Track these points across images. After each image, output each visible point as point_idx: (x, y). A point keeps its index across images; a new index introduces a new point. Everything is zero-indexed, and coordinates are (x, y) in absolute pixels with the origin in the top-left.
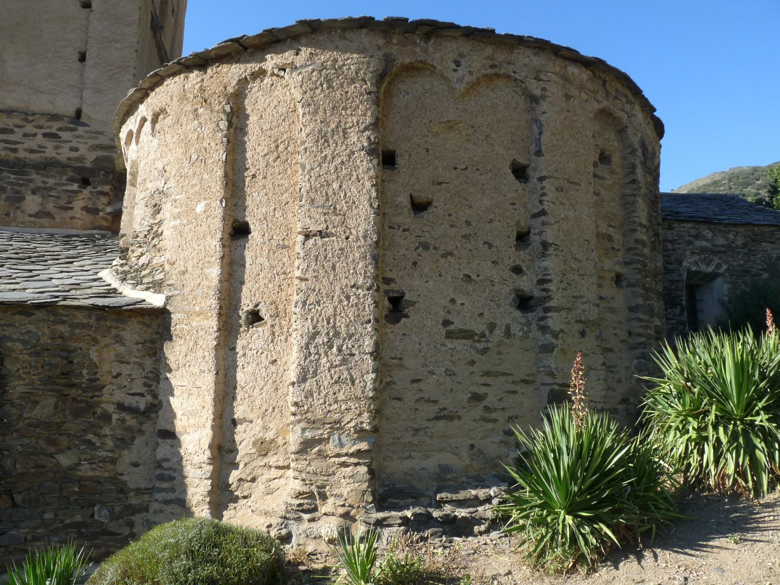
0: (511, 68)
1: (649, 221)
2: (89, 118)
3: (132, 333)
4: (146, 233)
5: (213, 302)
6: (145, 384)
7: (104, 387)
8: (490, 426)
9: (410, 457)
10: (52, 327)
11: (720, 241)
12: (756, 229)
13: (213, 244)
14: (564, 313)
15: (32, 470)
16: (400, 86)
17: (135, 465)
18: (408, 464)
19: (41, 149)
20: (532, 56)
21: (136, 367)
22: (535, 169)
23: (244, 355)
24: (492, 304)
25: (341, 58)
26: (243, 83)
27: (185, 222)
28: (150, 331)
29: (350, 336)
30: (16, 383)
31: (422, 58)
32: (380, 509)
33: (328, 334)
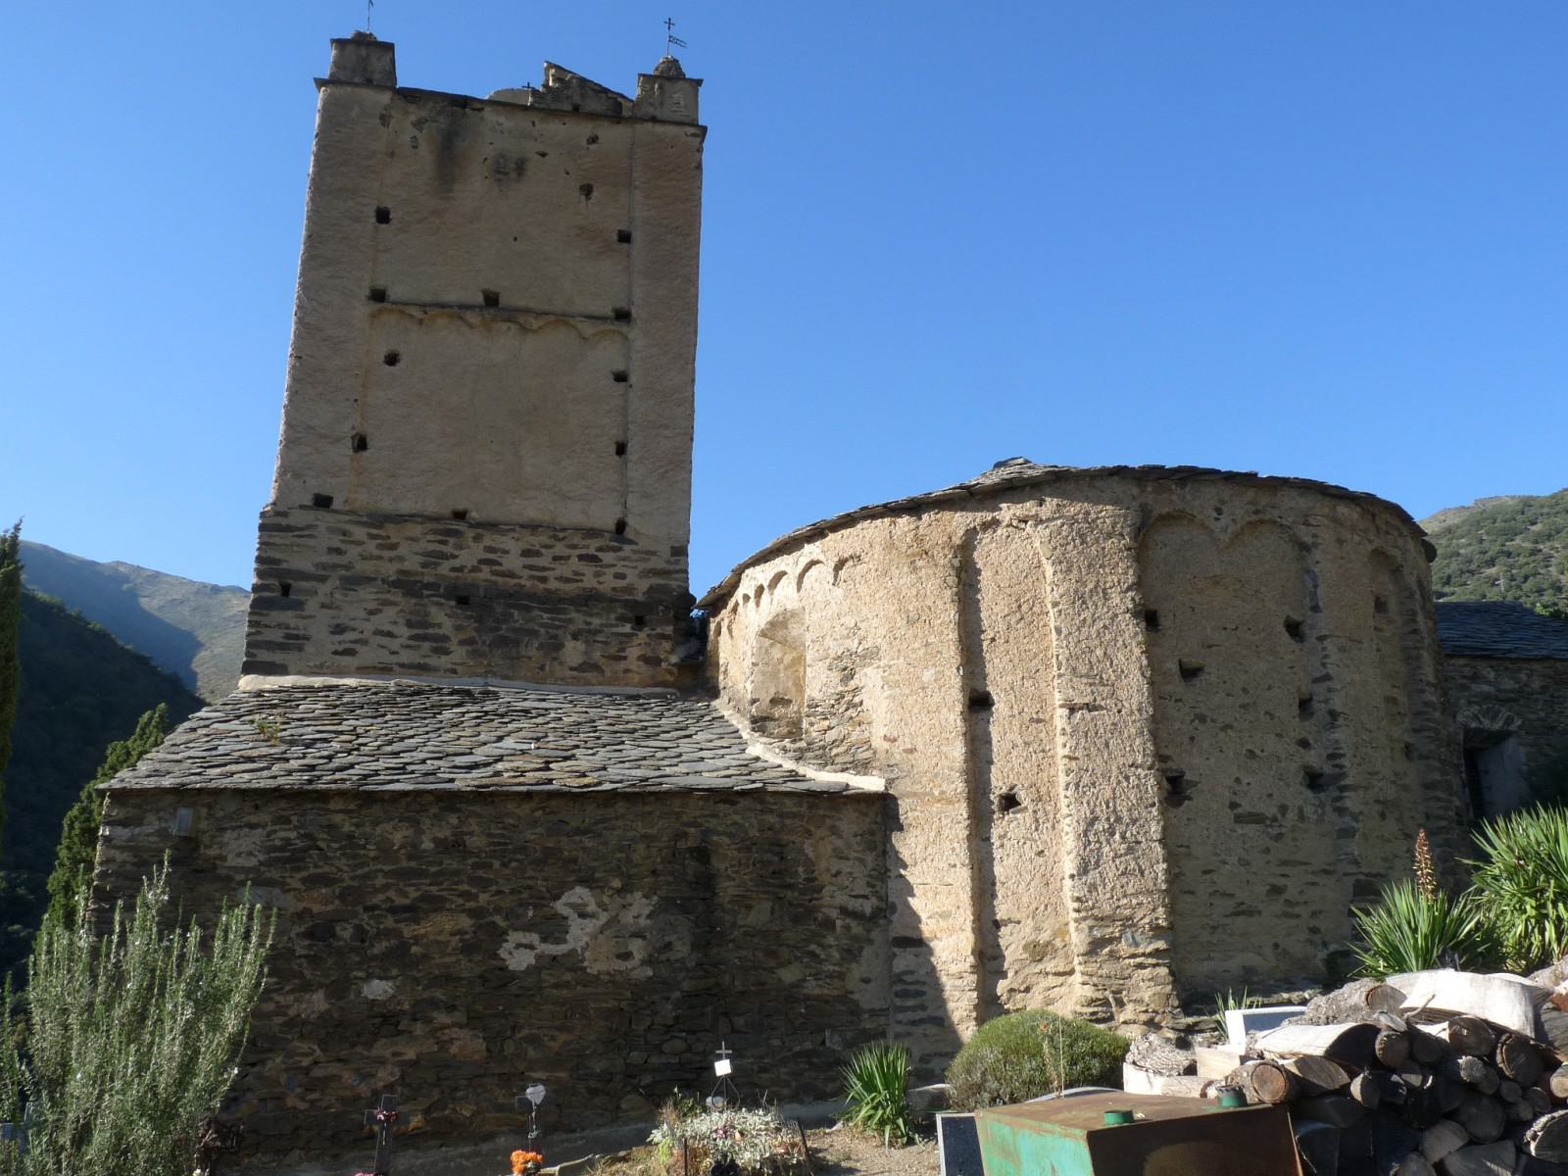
0: (1276, 513)
1: (1436, 677)
2: (637, 533)
3: (849, 823)
4: (833, 702)
5: (959, 786)
6: (869, 885)
7: (823, 887)
8: (1293, 922)
9: (1210, 958)
10: (760, 817)
11: (1508, 684)
12: (1559, 665)
13: (952, 717)
14: (1361, 792)
15: (753, 988)
16: (1155, 537)
17: (866, 981)
18: (1206, 967)
20: (1298, 498)
21: (857, 863)
22: (1312, 627)
23: (1002, 846)
24: (1281, 783)
25: (1093, 510)
26: (971, 534)
27: (907, 691)
28: (868, 820)
29: (1134, 821)
30: (726, 884)
31: (1180, 507)
32: (1188, 1014)
33: (1108, 819)
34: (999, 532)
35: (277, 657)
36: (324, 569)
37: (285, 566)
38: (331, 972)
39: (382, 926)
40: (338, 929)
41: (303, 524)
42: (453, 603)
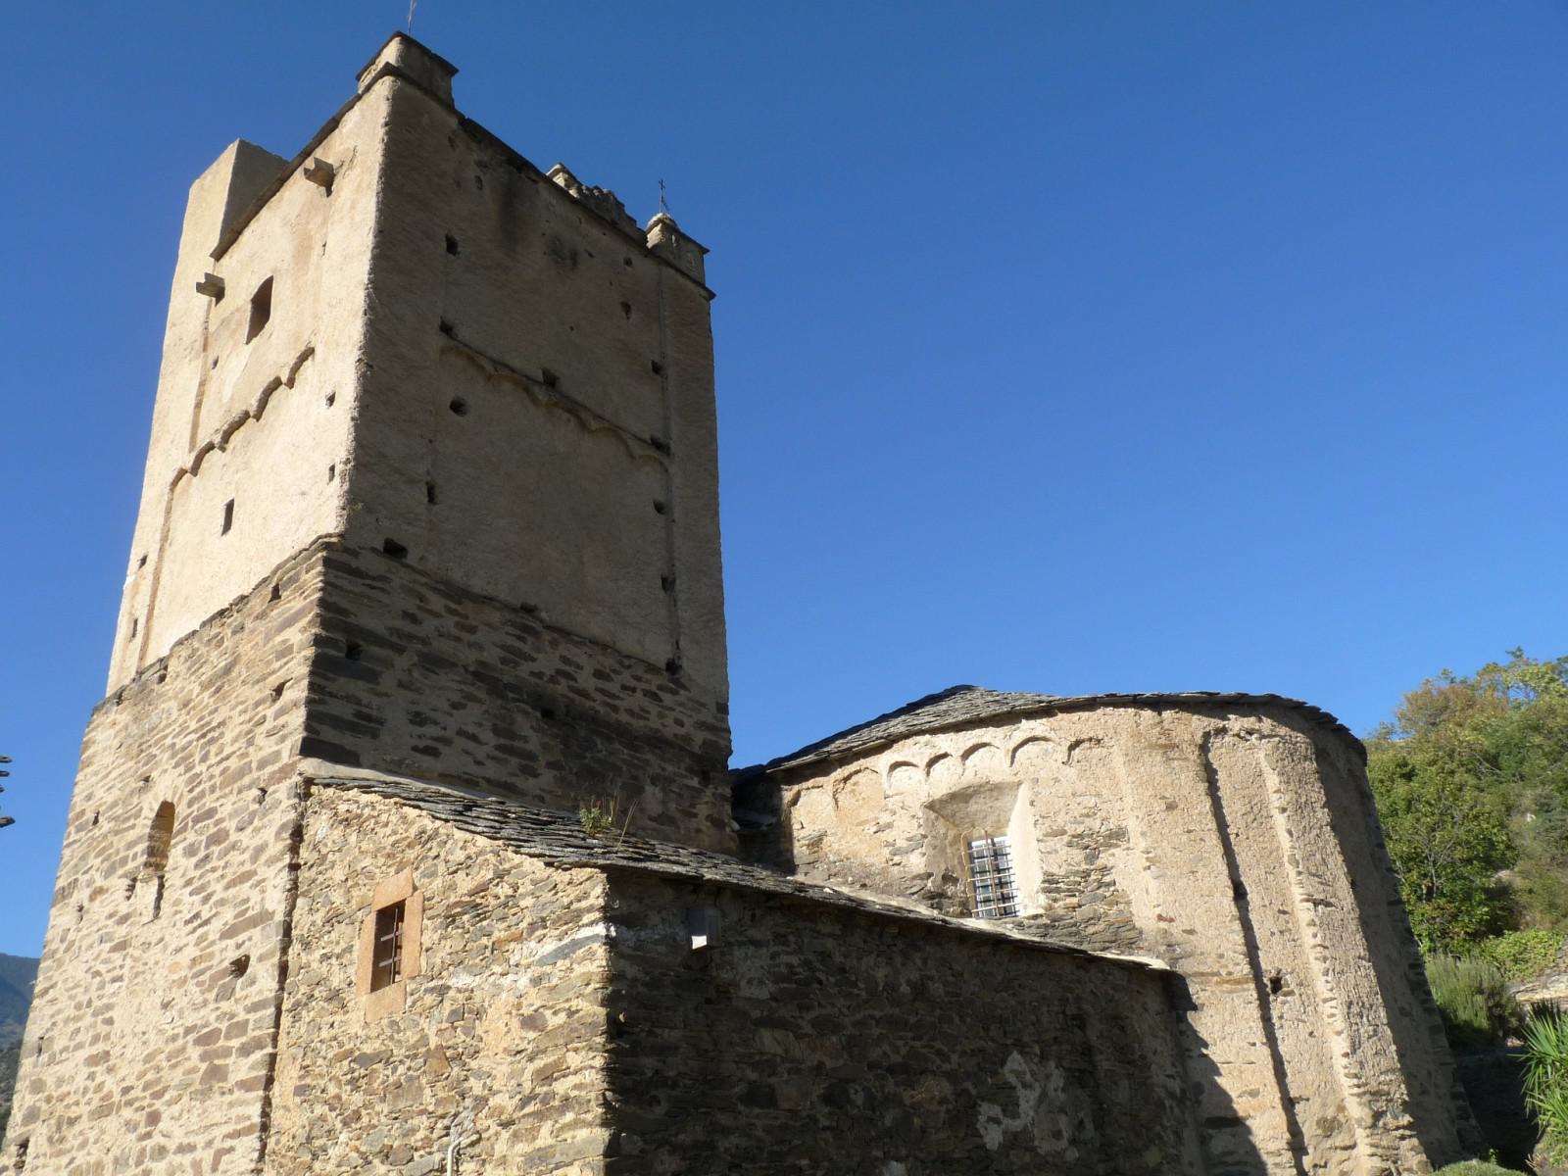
5: (1246, 969)
19: (641, 714)
23: (1282, 1027)
34: (1227, 739)
35: (347, 740)
36: (399, 637)
37: (352, 620)
42: (538, 714)
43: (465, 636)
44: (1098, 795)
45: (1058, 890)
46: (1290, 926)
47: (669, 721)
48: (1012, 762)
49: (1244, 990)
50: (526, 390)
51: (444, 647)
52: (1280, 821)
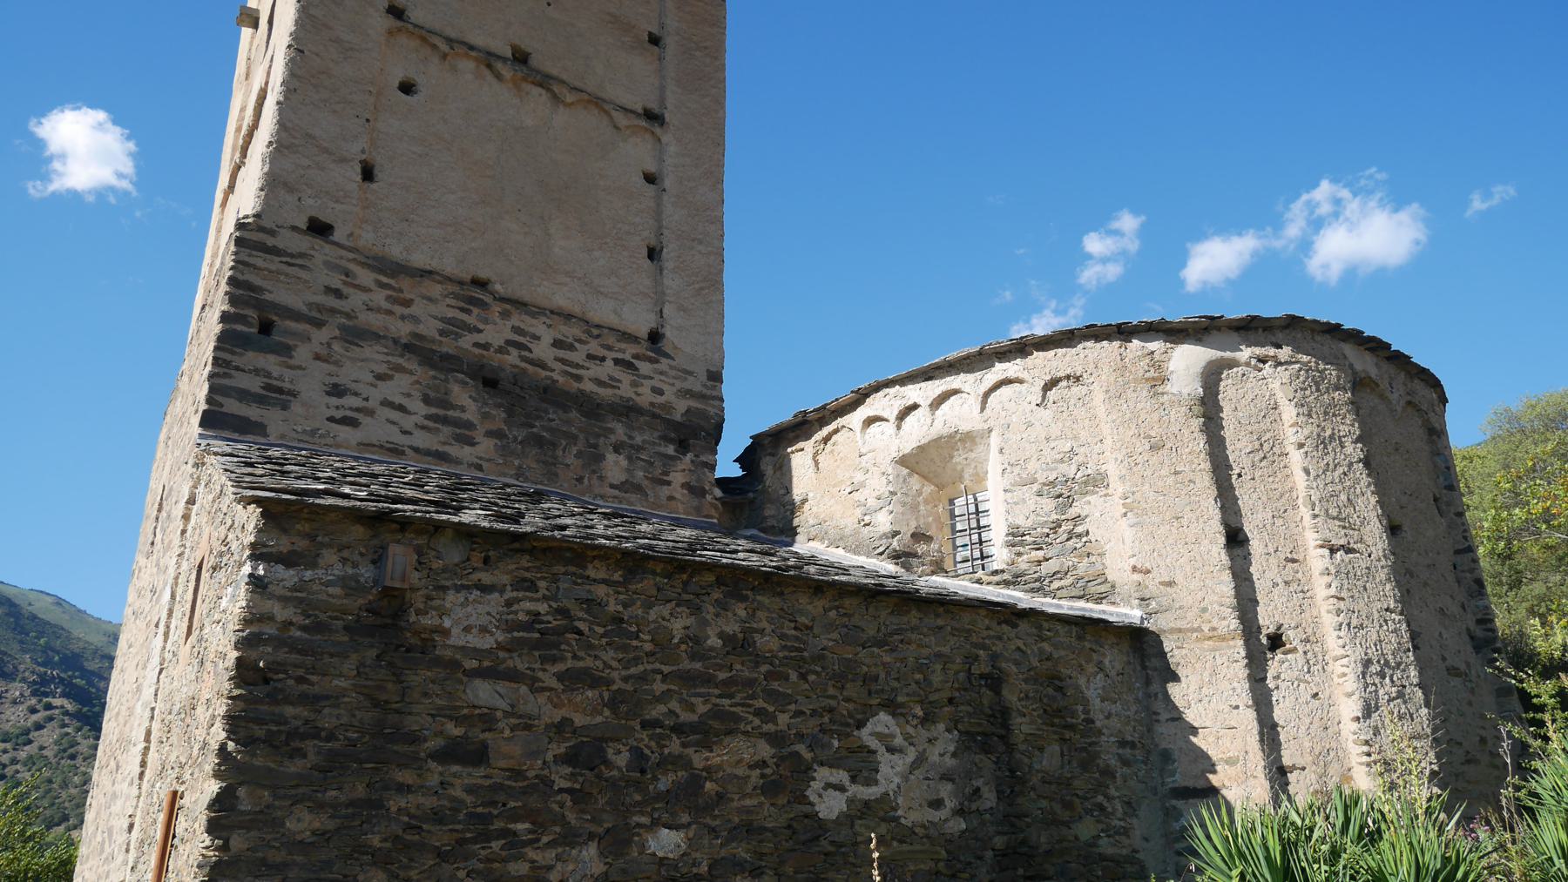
5: (1234, 623)
19: (612, 383)
37: (267, 296)
38: (605, 816)
39: (666, 751)
40: (610, 751)
41: (293, 249)
43: (398, 310)
44: (1075, 438)
45: (1022, 544)
46: (1300, 575)
47: (645, 390)
48: (983, 409)
49: (1230, 647)
50: (489, 66)
51: (374, 321)
52: (1296, 458)
